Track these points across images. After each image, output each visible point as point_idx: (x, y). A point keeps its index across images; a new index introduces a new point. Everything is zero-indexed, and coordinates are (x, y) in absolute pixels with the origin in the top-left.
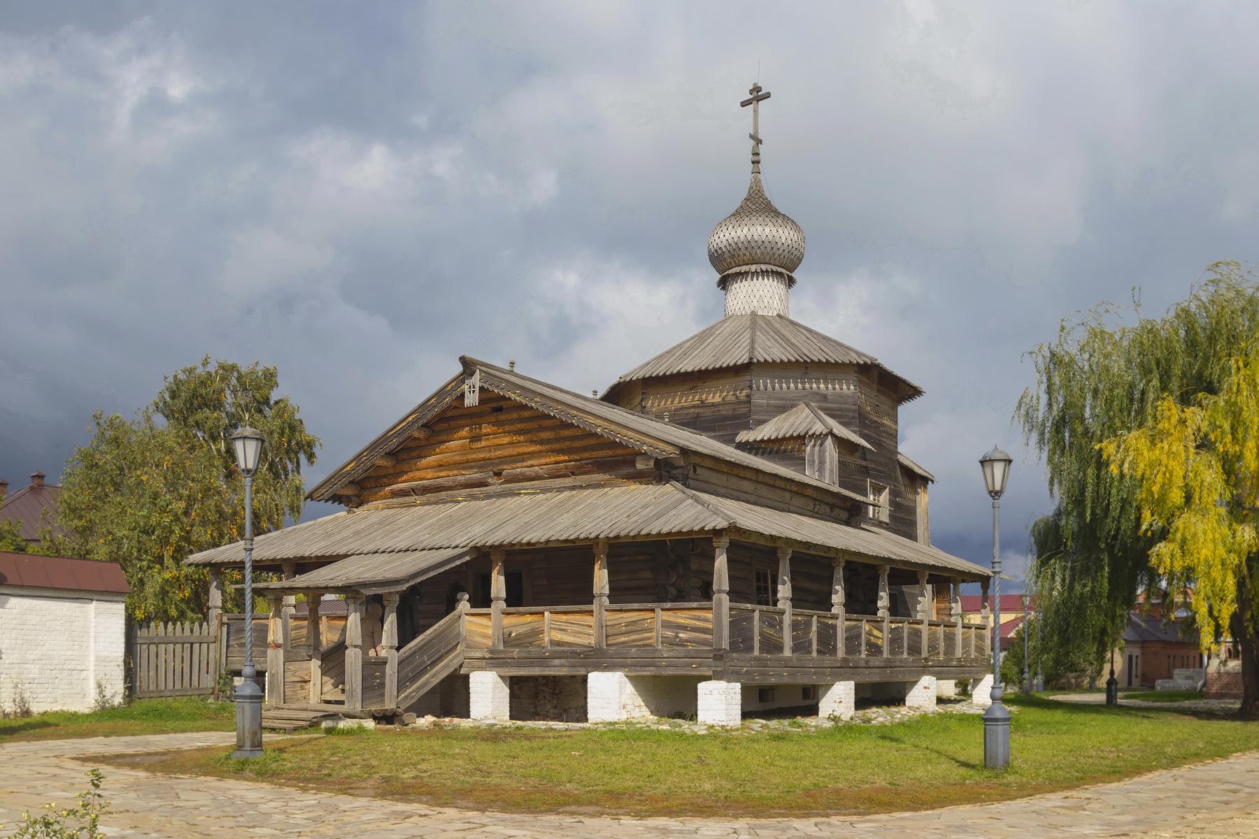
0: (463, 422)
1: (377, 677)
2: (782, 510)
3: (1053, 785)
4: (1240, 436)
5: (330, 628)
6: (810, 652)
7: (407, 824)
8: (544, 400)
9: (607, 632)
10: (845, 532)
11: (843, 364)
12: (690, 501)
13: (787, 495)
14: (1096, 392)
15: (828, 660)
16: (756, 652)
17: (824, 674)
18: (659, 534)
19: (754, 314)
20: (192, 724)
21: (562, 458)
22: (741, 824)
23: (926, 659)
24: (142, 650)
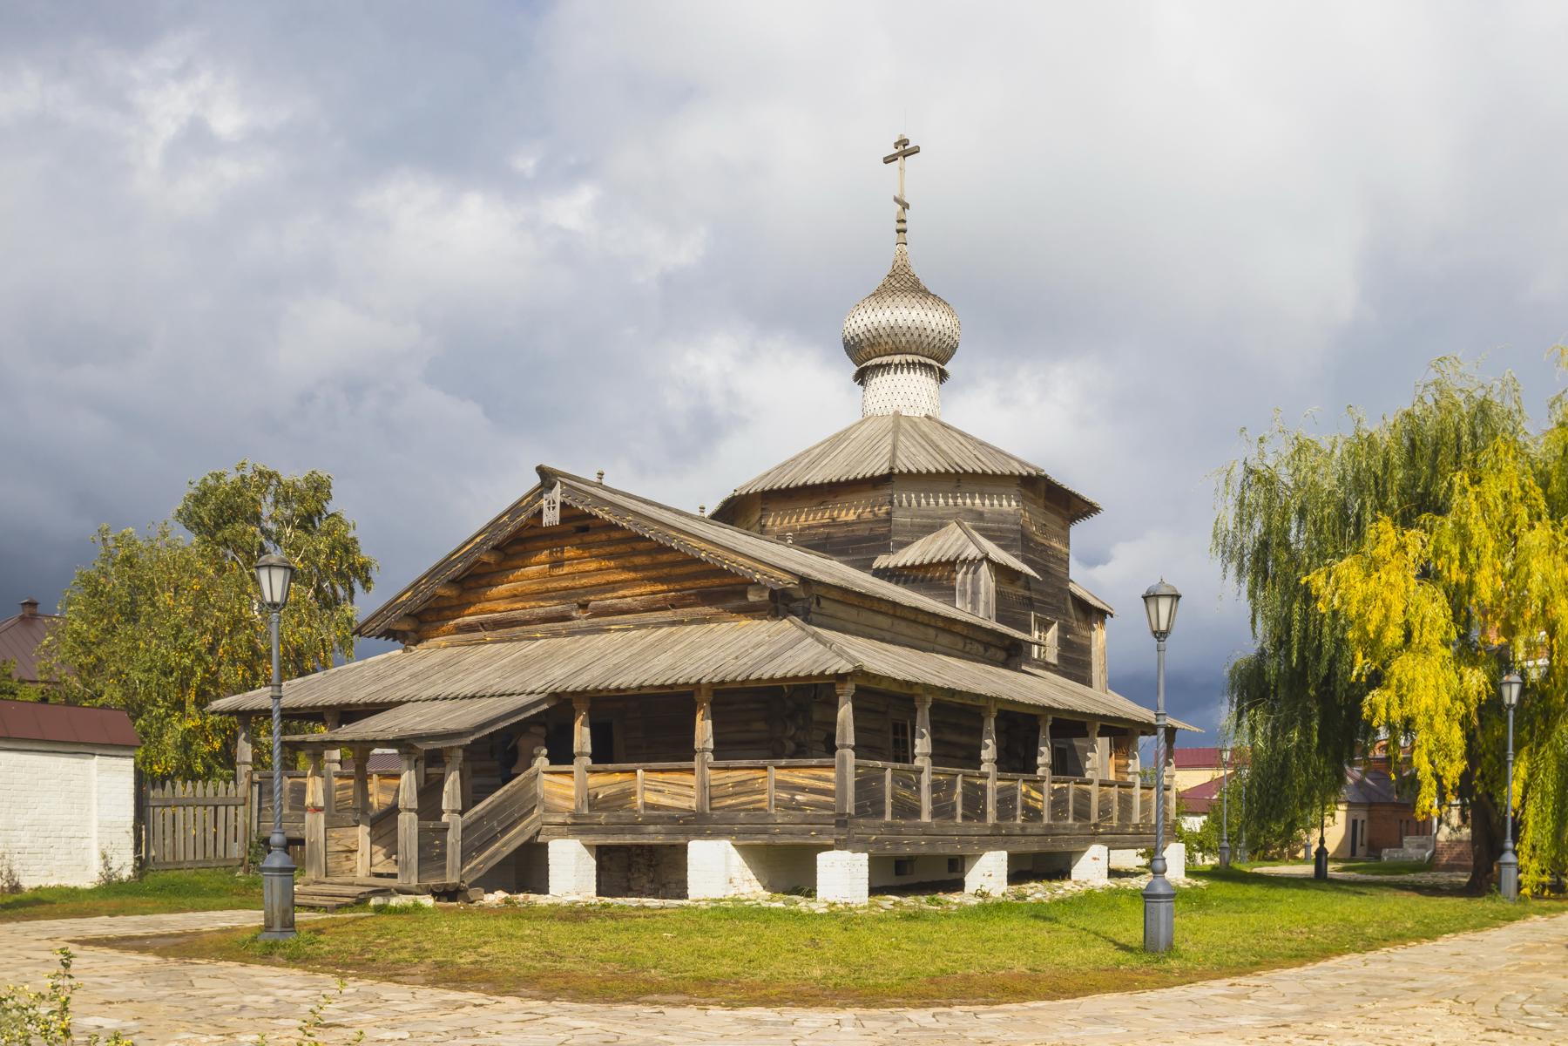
0: (540, 544)
1: (436, 847)
2: (924, 650)
3: (1223, 970)
4: (1472, 560)
5: (383, 789)
6: (953, 817)
7: (458, 1014)
8: (637, 520)
9: (710, 793)
10: (1004, 677)
11: (1003, 476)
12: (809, 640)
13: (932, 632)
14: (1302, 513)
15: (975, 826)
16: (888, 818)
17: (969, 843)
18: (771, 679)
19: (897, 415)
20: (215, 901)
21: (660, 587)
22: (848, 1014)
23: (1096, 825)
24: (158, 816)
